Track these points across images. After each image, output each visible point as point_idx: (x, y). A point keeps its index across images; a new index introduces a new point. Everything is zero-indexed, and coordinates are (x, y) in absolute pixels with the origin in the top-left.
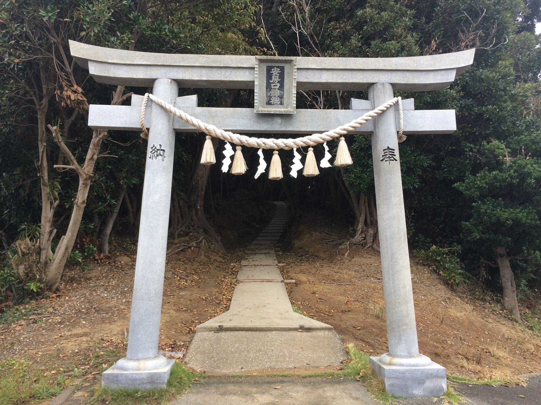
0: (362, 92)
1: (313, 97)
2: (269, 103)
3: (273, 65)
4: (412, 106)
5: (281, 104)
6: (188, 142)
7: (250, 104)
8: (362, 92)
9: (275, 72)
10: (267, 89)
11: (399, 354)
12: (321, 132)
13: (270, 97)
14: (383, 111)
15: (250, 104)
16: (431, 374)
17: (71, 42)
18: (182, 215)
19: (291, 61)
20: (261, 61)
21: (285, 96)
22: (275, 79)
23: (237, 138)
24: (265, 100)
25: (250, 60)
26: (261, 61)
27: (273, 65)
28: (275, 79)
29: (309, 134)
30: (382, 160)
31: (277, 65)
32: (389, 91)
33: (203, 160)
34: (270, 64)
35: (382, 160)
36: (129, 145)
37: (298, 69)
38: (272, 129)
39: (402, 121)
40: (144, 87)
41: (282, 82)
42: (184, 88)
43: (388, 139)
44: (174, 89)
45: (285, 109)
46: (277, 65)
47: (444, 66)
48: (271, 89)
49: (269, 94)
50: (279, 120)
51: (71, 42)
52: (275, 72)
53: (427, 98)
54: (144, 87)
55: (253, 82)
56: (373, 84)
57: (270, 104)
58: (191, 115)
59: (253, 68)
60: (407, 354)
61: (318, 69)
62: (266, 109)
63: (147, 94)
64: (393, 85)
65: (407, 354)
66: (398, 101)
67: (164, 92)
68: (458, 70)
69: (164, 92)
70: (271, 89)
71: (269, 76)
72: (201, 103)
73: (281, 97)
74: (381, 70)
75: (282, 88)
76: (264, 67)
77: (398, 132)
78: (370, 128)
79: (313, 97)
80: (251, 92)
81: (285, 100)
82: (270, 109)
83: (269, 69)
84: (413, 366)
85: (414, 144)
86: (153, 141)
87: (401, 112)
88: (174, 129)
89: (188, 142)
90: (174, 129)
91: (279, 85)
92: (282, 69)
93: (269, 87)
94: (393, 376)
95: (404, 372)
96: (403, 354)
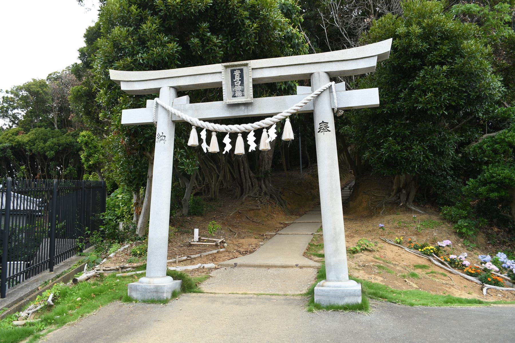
0: (306, 81)
1: (265, 88)
2: (234, 96)
3: (235, 68)
4: (344, 88)
5: (243, 96)
6: (182, 129)
7: (220, 98)
8: (306, 81)
9: (237, 73)
10: (232, 86)
11: (330, 279)
12: (271, 116)
13: (235, 92)
14: (319, 95)
15: (220, 98)
16: (350, 293)
17: (391, 39)
18: (252, 184)
19: (246, 65)
20: (226, 67)
21: (245, 90)
22: (237, 78)
23: (201, 124)
24: (231, 94)
25: (218, 67)
26: (226, 67)
27: (235, 68)
28: (237, 78)
29: (276, 114)
30: (319, 132)
31: (238, 68)
32: (326, 78)
33: (190, 143)
34: (233, 68)
35: (319, 132)
36: (145, 134)
37: (252, 69)
38: (238, 115)
39: (335, 101)
40: (154, 94)
41: (242, 80)
42: (180, 92)
43: (324, 115)
44: (173, 92)
45: (246, 100)
46: (238, 68)
47: (367, 55)
48: (235, 86)
49: (233, 90)
50: (243, 108)
51: (391, 39)
52: (237, 73)
53: (354, 80)
54: (154, 94)
55: (222, 82)
56: (311, 74)
57: (235, 97)
58: (178, 110)
59: (221, 72)
60: (335, 279)
61: (270, 67)
62: (232, 101)
63: (156, 99)
64: (328, 73)
65: (335, 279)
66: (331, 86)
67: (166, 97)
68: (379, 56)
69: (166, 97)
70: (235, 86)
71: (233, 77)
72: (192, 101)
73: (242, 91)
74: (320, 64)
75: (242, 84)
76: (229, 70)
77: (333, 109)
78: (310, 108)
79: (265, 88)
80: (220, 90)
81: (245, 93)
82: (234, 101)
83: (232, 72)
84: (337, 287)
85: (344, 118)
86: (159, 131)
87: (334, 93)
88: (173, 121)
89: (182, 129)
90: (173, 121)
91: (240, 82)
92: (242, 70)
93: (233, 85)
94: (127, 279)
95: (328, 292)
96: (333, 279)
